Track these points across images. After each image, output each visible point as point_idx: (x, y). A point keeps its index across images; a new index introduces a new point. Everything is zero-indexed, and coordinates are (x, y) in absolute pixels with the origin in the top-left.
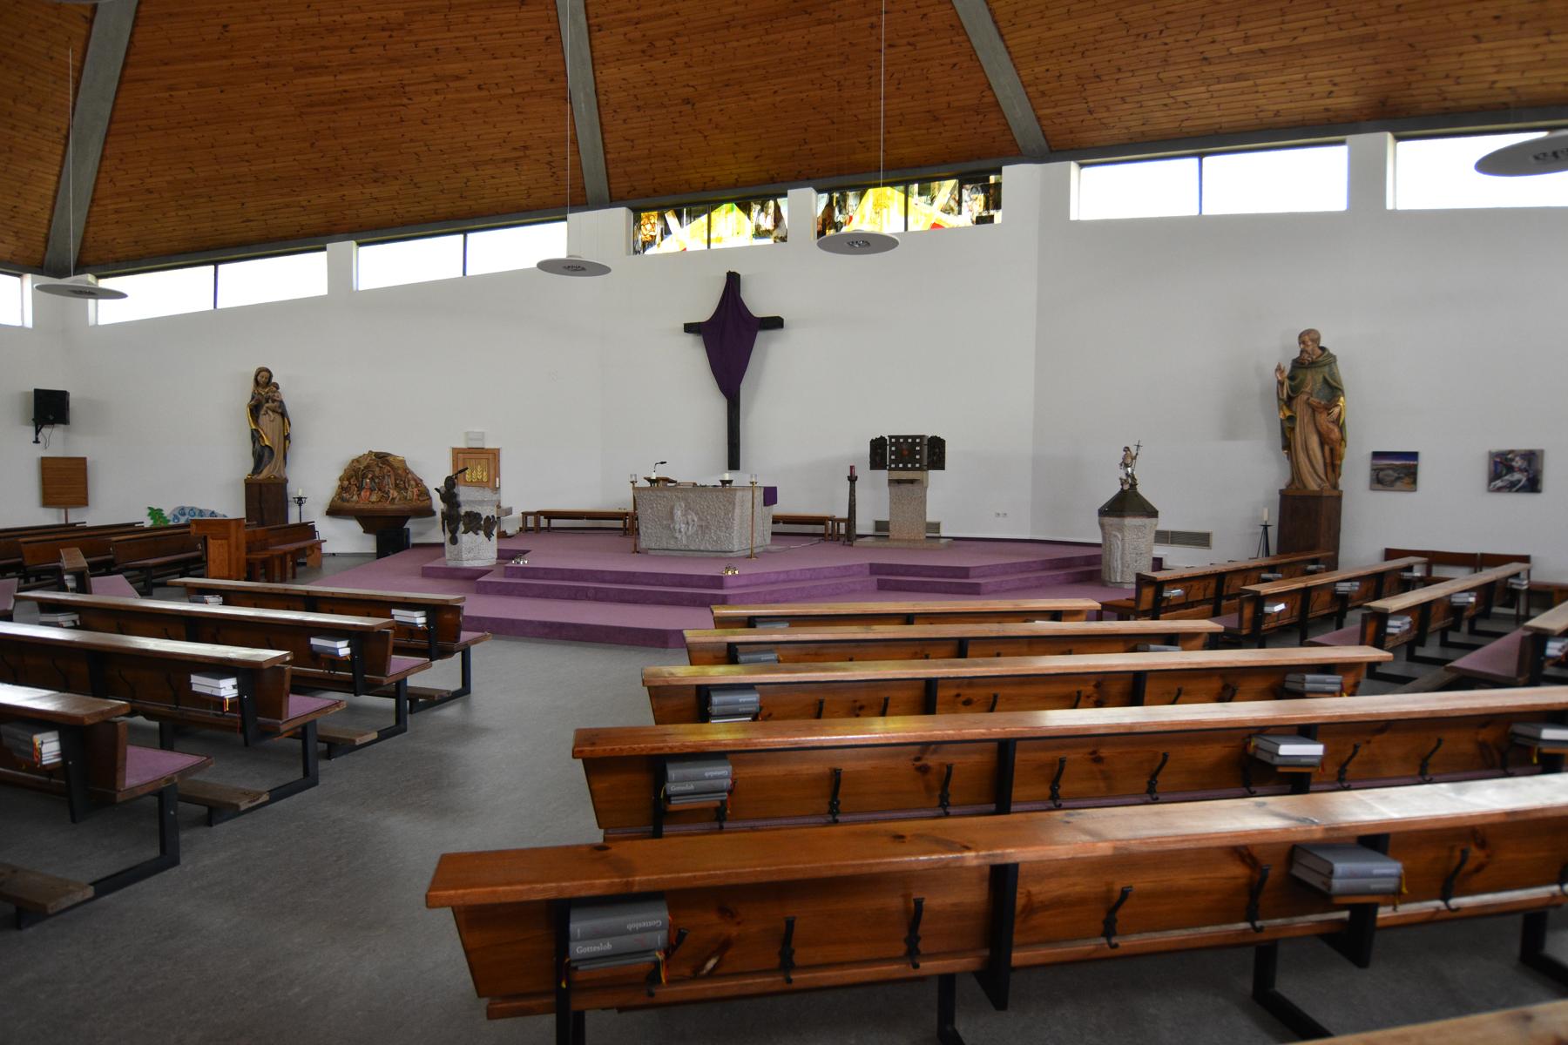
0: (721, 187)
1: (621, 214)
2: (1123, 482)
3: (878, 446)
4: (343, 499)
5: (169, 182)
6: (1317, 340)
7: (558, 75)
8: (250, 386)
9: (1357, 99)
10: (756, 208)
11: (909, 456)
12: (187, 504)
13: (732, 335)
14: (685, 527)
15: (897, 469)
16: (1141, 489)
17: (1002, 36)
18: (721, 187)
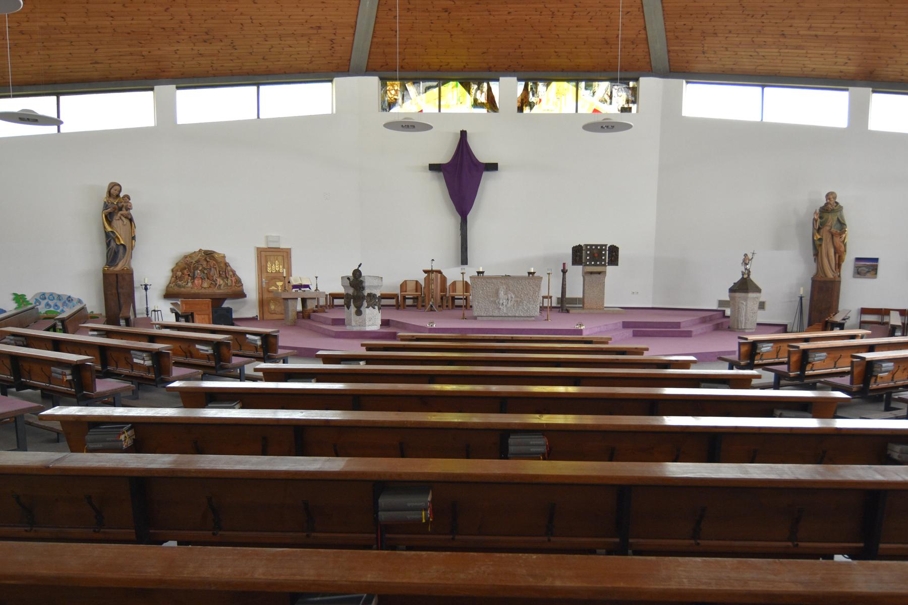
0: (451, 70)
1: (373, 81)
2: (743, 274)
4: (179, 286)
5: (42, 27)
6: (835, 198)
8: (104, 194)
10: (474, 87)
11: (595, 257)
12: (47, 290)
13: (462, 174)
14: (506, 302)
15: (590, 265)
16: (752, 277)
18: (451, 70)
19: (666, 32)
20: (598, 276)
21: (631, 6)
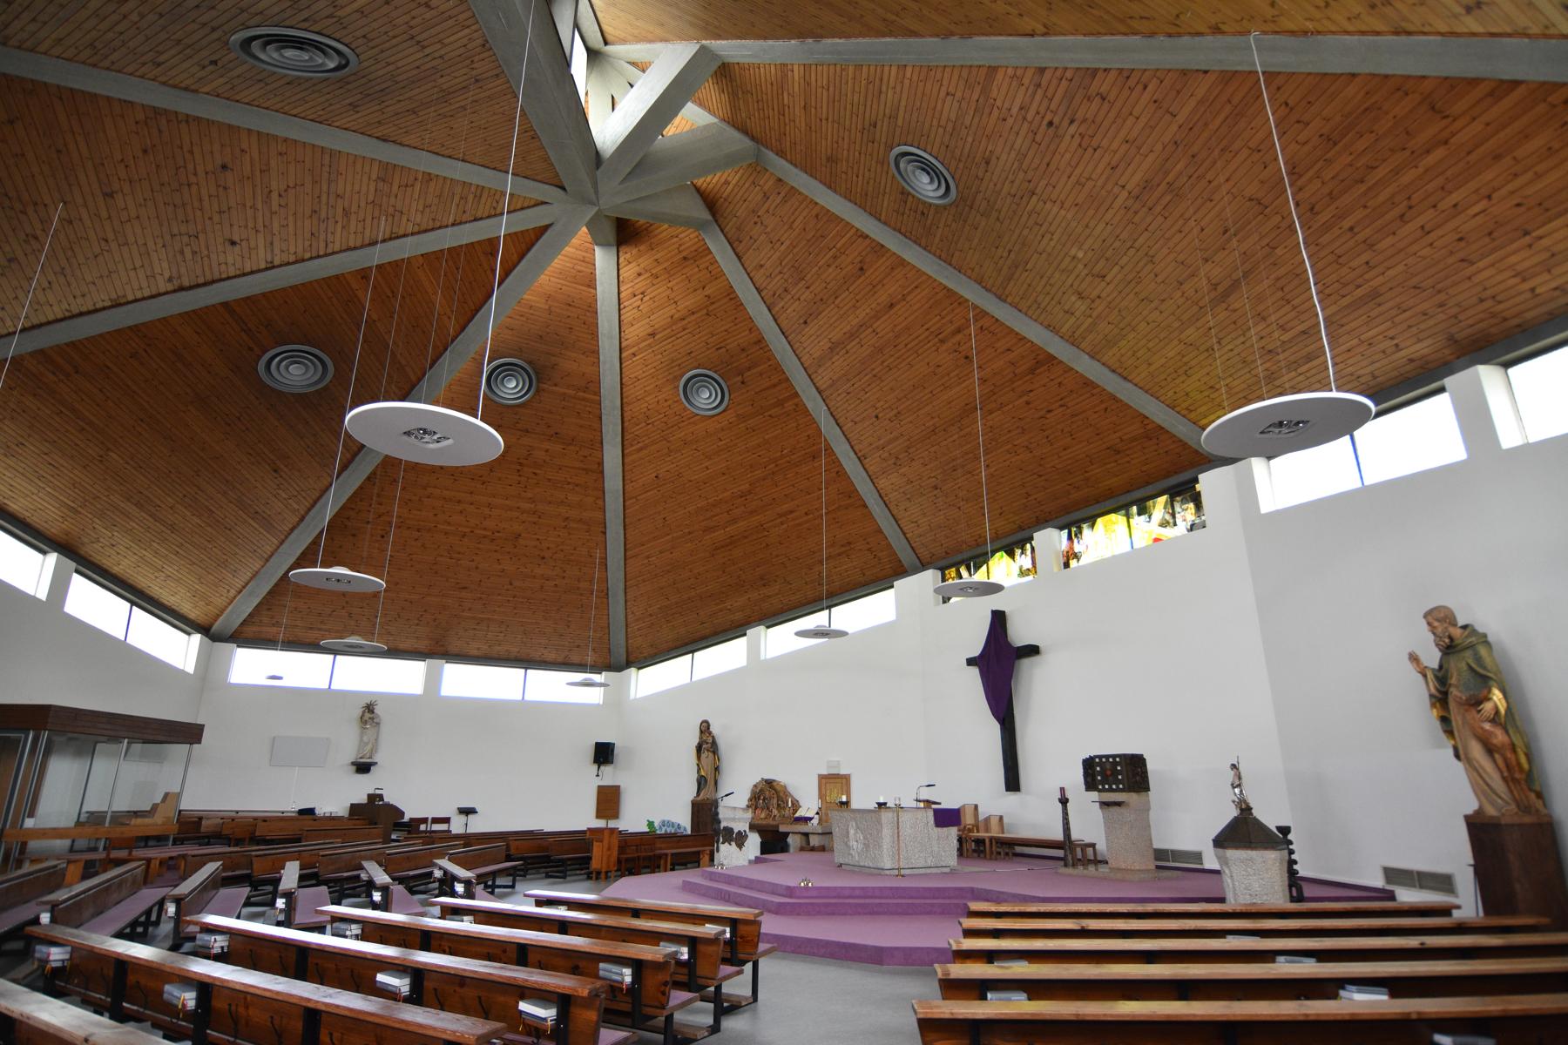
3: (1089, 764)
7: (852, 493)
9: (1425, 343)
10: (1018, 552)
13: (1001, 661)
15: (1104, 790)
20: (1116, 809)
21: (1482, 301)
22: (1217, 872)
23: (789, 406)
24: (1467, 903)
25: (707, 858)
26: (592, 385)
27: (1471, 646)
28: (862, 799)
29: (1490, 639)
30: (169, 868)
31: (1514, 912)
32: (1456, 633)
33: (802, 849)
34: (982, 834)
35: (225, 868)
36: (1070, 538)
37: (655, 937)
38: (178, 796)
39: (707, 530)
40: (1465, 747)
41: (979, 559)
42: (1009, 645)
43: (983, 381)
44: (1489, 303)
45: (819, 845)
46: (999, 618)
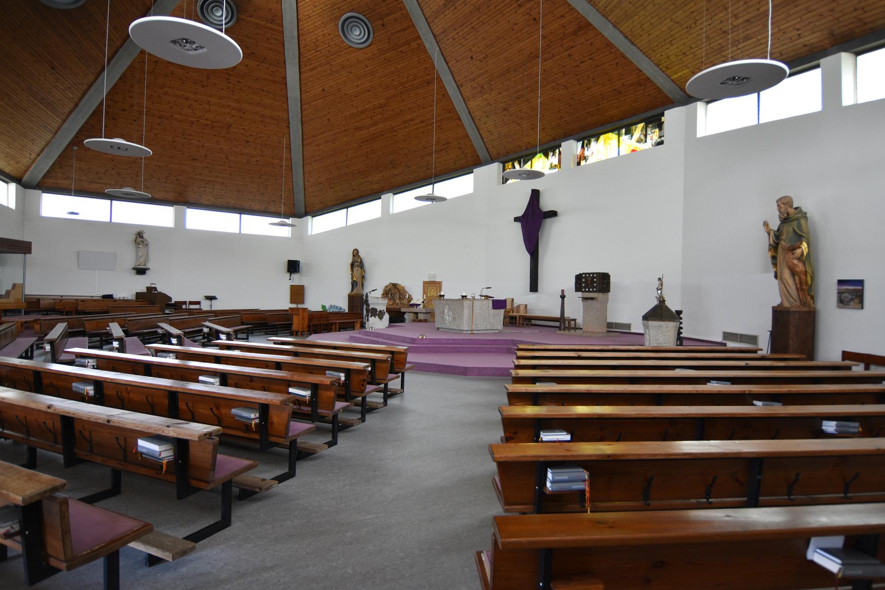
3: (579, 278)
7: (452, 110)
9: (816, 35)
10: (551, 154)
13: (534, 220)
15: (585, 291)
17: (633, 43)
19: (658, 66)
20: (591, 301)
21: (856, 10)
22: (643, 334)
23: (414, 45)
24: (764, 345)
25: (359, 325)
26: (277, 19)
27: (798, 219)
28: (450, 292)
29: (808, 215)
30: (26, 328)
31: (786, 352)
32: (791, 211)
33: (414, 321)
34: (515, 314)
35: (70, 326)
36: (583, 147)
37: (322, 370)
38: (23, 286)
39: (357, 129)
40: (781, 273)
41: (530, 157)
42: (540, 210)
43: (544, 37)
44: (859, 12)
45: (426, 317)
46: (535, 195)
